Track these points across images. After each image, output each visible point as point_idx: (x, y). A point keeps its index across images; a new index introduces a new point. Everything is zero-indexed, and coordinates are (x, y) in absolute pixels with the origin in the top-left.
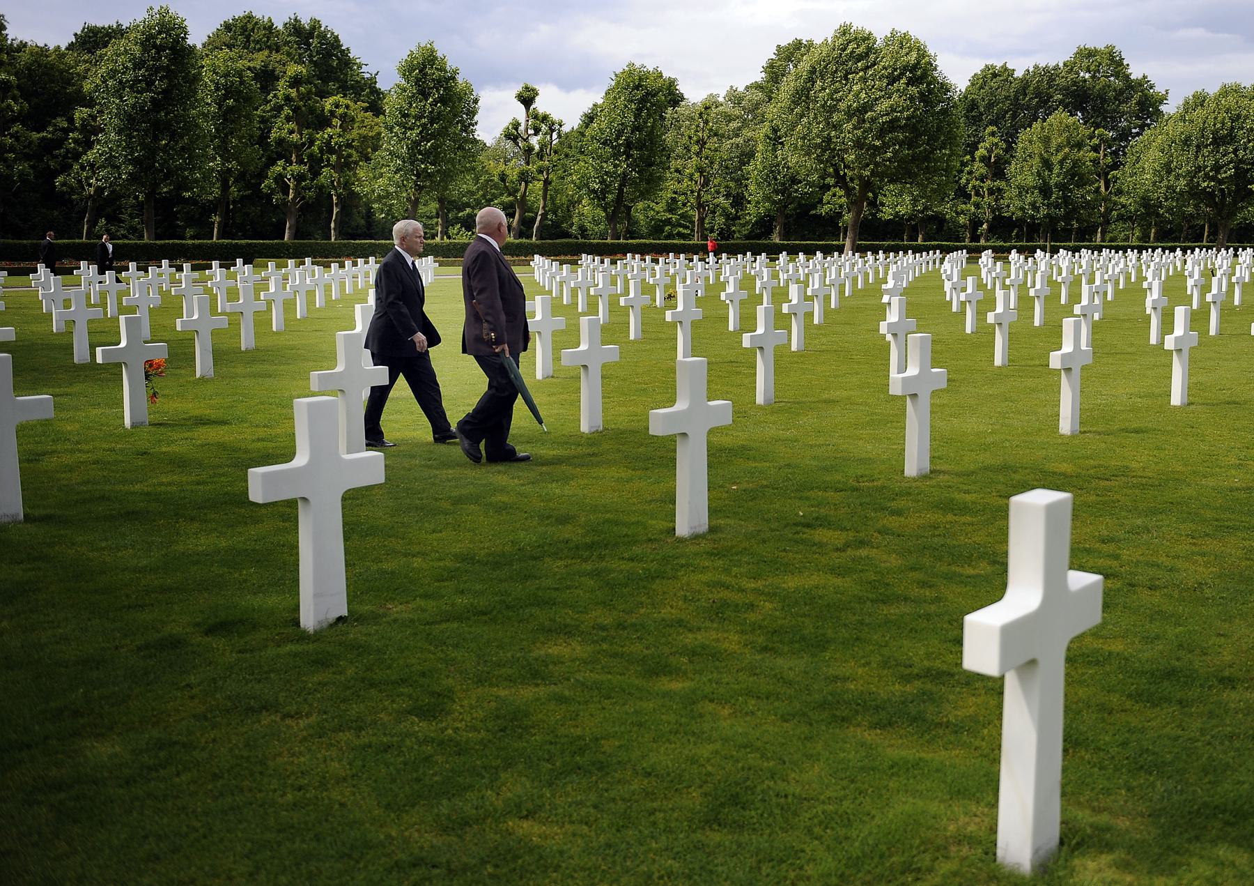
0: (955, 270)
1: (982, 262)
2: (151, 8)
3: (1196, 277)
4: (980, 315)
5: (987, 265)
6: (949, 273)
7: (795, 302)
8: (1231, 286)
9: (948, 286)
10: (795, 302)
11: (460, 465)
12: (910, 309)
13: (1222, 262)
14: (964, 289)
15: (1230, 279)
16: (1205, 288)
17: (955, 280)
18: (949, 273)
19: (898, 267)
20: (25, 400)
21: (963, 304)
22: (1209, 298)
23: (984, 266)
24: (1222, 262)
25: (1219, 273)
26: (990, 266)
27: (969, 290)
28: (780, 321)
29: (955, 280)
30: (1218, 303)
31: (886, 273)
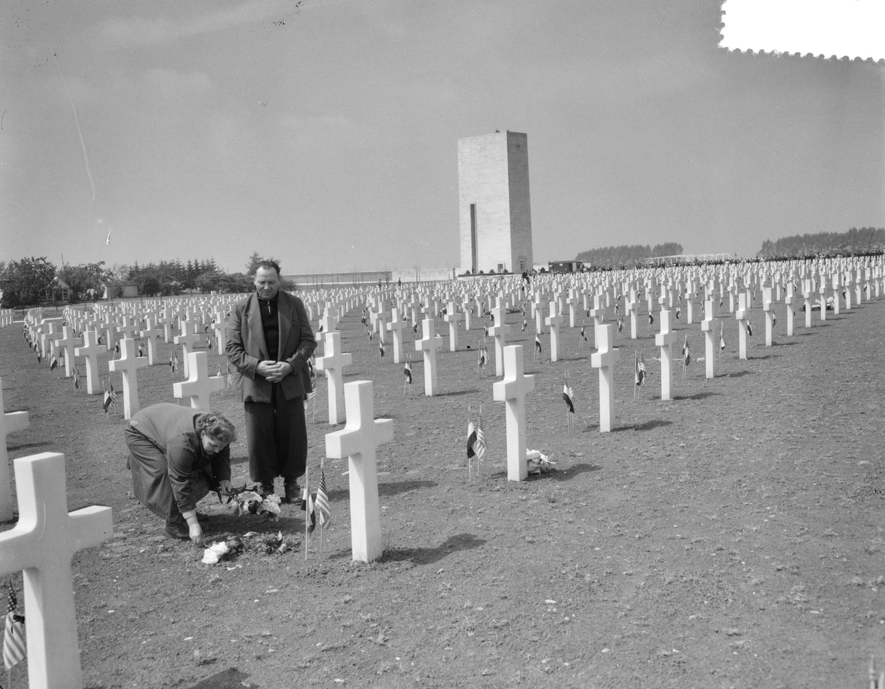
0: (380, 304)
1: (398, 296)
2: (103, 263)
3: (537, 302)
4: (407, 344)
5: (402, 298)
6: (374, 306)
7: (193, 378)
8: (566, 306)
9: (373, 318)
10: (193, 378)
11: (298, 276)
12: (344, 343)
13: (557, 287)
14: (390, 319)
15: (564, 301)
16: (545, 313)
17: (381, 311)
18: (374, 306)
19: (332, 304)
20: (11, 415)
21: (389, 333)
22: (548, 322)
23: (420, 292)
24: (557, 287)
25: (556, 295)
26: (405, 298)
27: (395, 320)
28: (440, 326)
29: (381, 311)
30: (557, 326)
31: (322, 311)
